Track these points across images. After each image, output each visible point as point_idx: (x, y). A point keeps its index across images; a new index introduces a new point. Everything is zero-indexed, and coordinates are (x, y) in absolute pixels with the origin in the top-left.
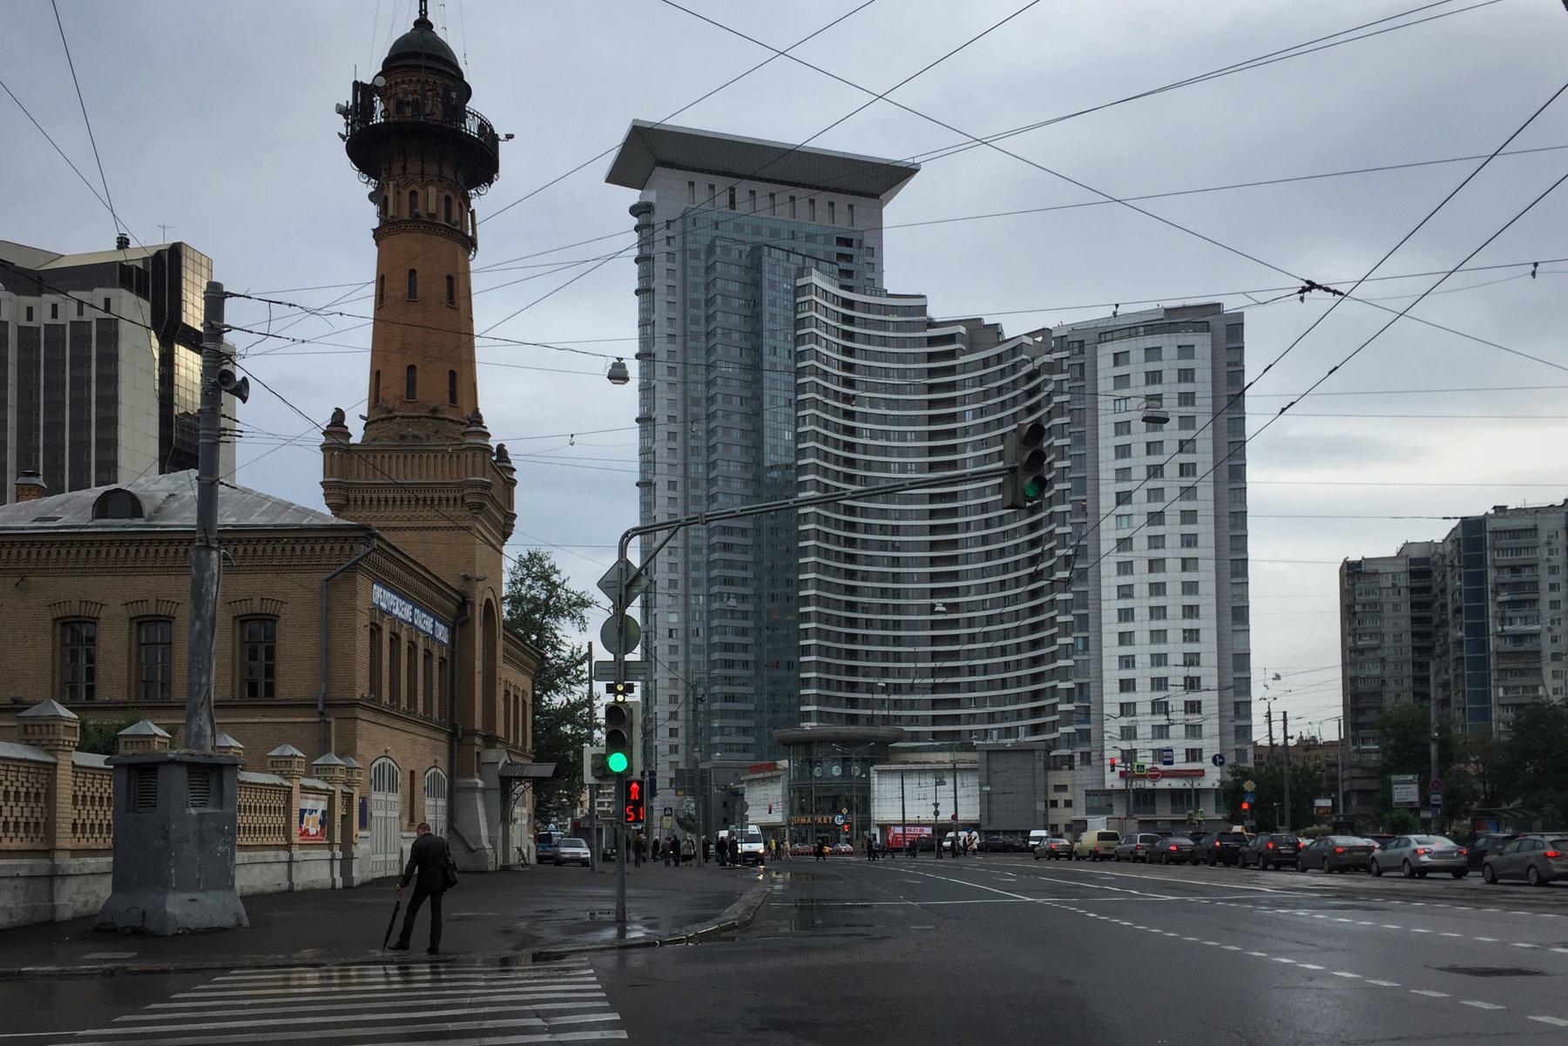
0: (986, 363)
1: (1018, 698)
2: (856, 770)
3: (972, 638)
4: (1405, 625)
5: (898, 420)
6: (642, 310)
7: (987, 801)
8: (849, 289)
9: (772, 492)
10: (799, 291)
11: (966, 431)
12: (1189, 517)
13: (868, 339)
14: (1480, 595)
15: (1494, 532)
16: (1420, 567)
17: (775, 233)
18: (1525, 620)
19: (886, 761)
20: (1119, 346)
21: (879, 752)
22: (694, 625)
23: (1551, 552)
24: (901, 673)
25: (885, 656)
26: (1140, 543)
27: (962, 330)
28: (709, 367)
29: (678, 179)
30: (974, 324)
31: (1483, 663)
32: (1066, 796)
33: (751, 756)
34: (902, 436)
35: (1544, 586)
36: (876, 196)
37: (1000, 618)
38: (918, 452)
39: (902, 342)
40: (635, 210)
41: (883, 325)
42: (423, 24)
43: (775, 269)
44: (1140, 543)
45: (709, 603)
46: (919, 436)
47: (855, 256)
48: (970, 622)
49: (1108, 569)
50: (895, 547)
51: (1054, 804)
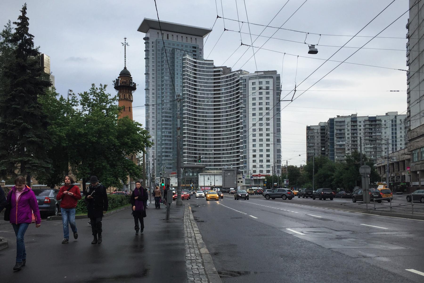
0: (227, 77)
1: (234, 157)
2: (195, 174)
3: (223, 142)
4: (320, 141)
5: (207, 90)
6: (146, 63)
7: (224, 181)
8: (195, 59)
9: (177, 101)
10: (184, 59)
11: (223, 93)
12: (268, 119)
13: (200, 71)
14: (333, 135)
15: (336, 122)
16: (323, 128)
17: (178, 45)
18: (342, 141)
19: (202, 172)
20: (253, 81)
21: (201, 170)
22: (158, 139)
23: (348, 126)
24: (207, 150)
25: (203, 146)
26: (257, 125)
27: (222, 69)
28: (162, 77)
29: (156, 31)
30: (225, 68)
31: (333, 151)
32: (241, 180)
33: (172, 170)
34: (208, 94)
35: (346, 134)
36: (202, 36)
37: (230, 138)
38: (211, 98)
39: (208, 72)
40: (144, 39)
41: (203, 68)
42: (125, 68)
43: (178, 55)
44: (257, 125)
45: (162, 134)
46: (212, 94)
47: (197, 51)
48: (223, 139)
49: (251, 131)
50: (206, 120)
51: (239, 182)
